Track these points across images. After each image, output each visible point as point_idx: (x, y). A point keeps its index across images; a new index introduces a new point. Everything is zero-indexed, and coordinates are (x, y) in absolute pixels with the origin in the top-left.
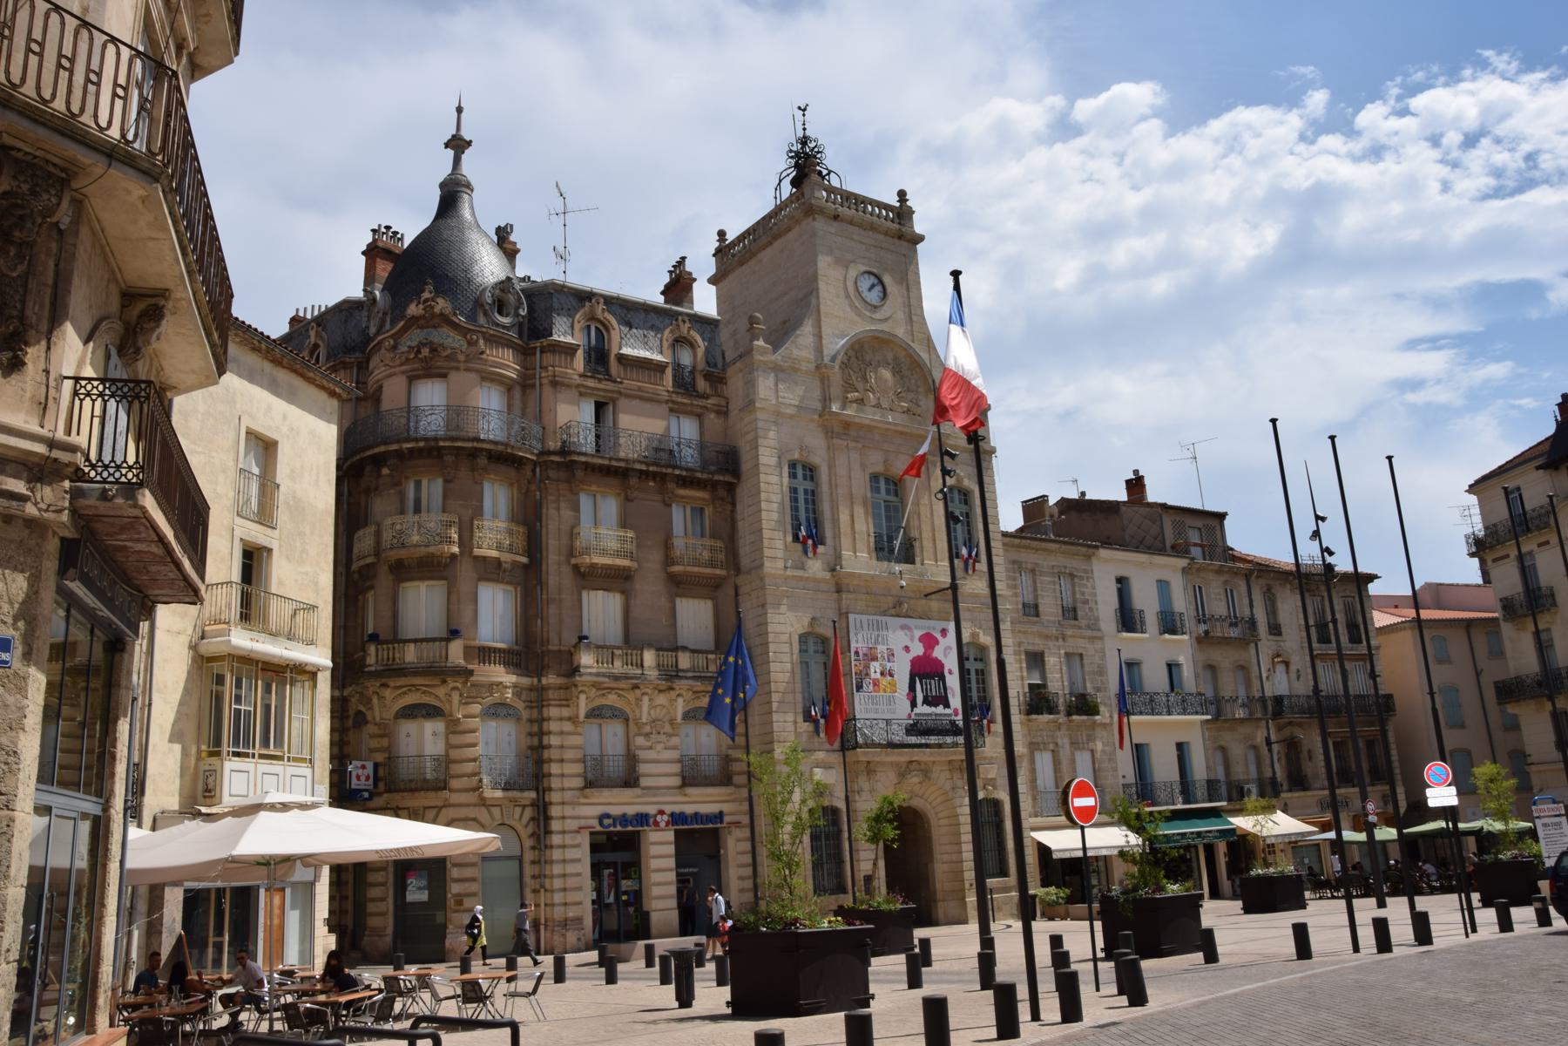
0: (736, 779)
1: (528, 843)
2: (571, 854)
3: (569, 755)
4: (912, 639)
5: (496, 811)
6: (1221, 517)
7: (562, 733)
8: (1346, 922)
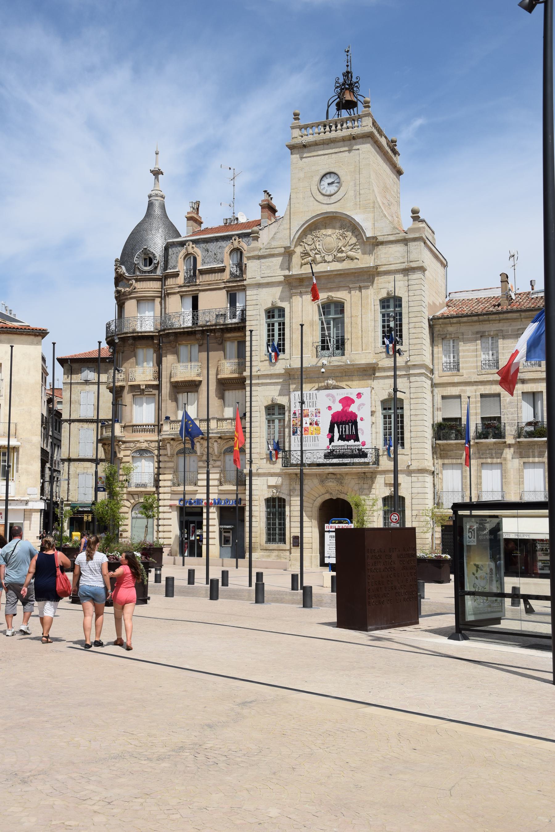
0: (200, 483)
4: (334, 402)
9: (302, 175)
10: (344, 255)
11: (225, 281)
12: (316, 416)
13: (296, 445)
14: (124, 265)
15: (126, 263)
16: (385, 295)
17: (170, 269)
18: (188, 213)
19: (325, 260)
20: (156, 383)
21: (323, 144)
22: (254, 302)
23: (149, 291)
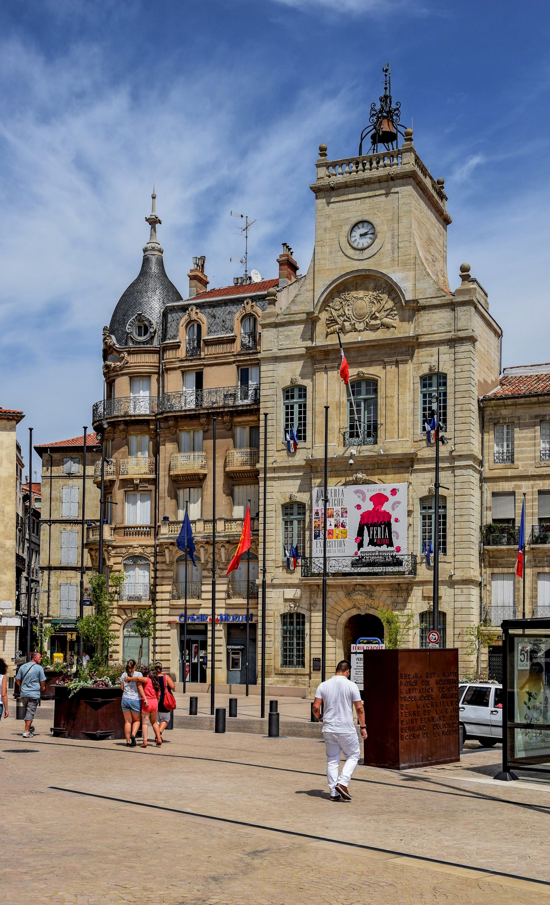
4: (364, 500)
7: (163, 570)
8: (216, 695)
9: (328, 224)
10: (378, 322)
11: (235, 353)
12: (342, 516)
13: (318, 551)
14: (114, 334)
15: (116, 332)
16: (426, 371)
17: (170, 339)
18: (191, 271)
19: (355, 328)
20: (152, 476)
21: (355, 186)
22: (270, 380)
23: (144, 366)
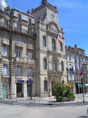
1: (8, 83)
2: (14, 87)
3: (14, 72)
5: (4, 79)
6: (84, 50)
7: (13, 69)
